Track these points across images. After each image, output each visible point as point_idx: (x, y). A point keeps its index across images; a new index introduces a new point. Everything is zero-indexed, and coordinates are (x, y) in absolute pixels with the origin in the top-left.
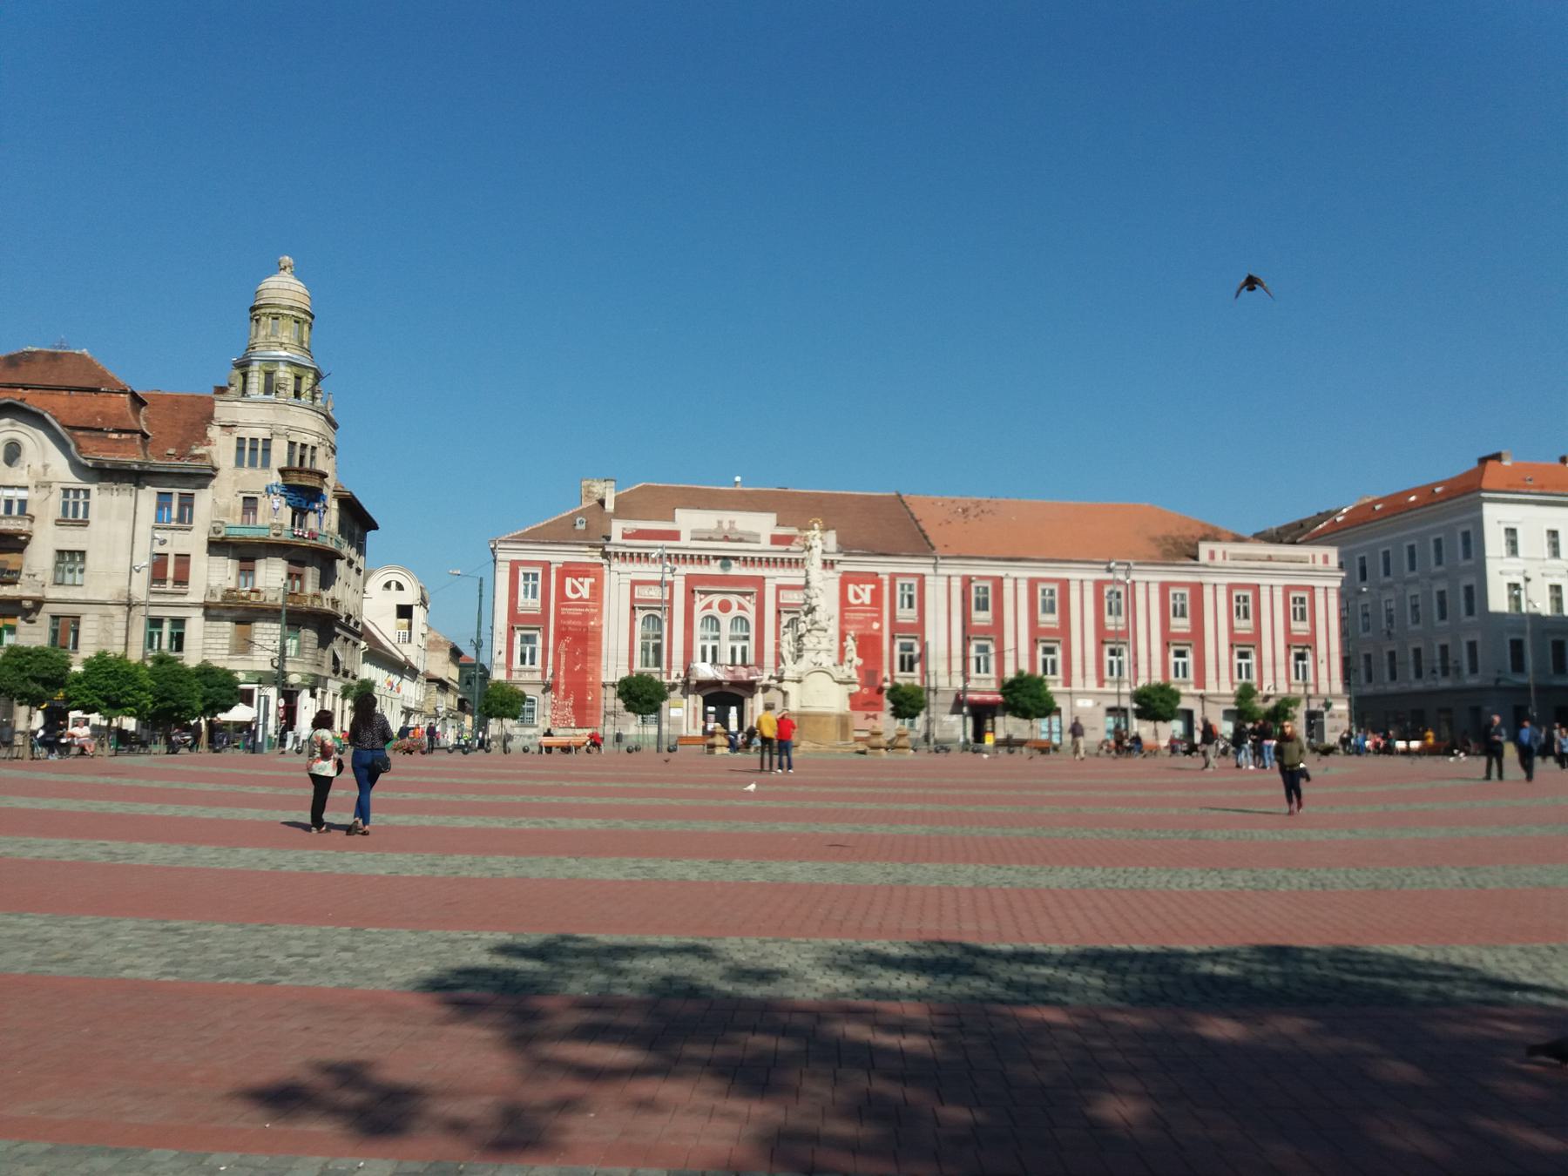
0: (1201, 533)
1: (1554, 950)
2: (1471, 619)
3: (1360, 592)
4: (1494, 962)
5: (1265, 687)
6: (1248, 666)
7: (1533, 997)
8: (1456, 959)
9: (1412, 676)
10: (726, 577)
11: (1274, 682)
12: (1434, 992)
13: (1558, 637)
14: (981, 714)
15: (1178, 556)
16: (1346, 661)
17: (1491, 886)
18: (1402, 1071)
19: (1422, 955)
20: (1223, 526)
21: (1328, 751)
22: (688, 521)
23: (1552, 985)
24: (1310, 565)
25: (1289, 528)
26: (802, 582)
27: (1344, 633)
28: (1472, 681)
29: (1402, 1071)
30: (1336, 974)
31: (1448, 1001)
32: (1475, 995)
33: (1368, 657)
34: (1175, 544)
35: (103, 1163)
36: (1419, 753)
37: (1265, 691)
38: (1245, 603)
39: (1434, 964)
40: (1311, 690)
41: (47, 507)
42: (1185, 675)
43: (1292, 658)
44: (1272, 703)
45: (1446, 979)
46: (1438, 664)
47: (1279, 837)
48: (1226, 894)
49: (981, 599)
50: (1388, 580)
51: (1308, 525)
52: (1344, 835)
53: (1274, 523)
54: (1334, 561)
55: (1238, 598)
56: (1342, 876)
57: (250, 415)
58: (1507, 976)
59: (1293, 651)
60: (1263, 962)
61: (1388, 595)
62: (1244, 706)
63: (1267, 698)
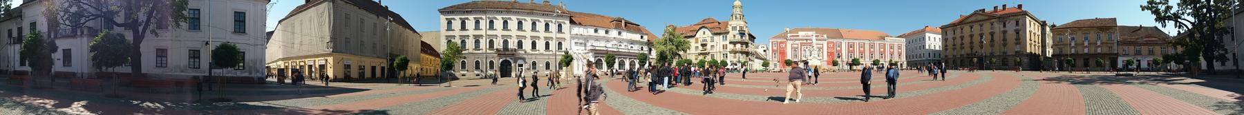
10: (807, 43)
11: (896, 59)
14: (851, 65)
22: (801, 33)
26: (525, 95)
35: (49, 103)
41: (709, 40)
49: (851, 46)
57: (733, 23)
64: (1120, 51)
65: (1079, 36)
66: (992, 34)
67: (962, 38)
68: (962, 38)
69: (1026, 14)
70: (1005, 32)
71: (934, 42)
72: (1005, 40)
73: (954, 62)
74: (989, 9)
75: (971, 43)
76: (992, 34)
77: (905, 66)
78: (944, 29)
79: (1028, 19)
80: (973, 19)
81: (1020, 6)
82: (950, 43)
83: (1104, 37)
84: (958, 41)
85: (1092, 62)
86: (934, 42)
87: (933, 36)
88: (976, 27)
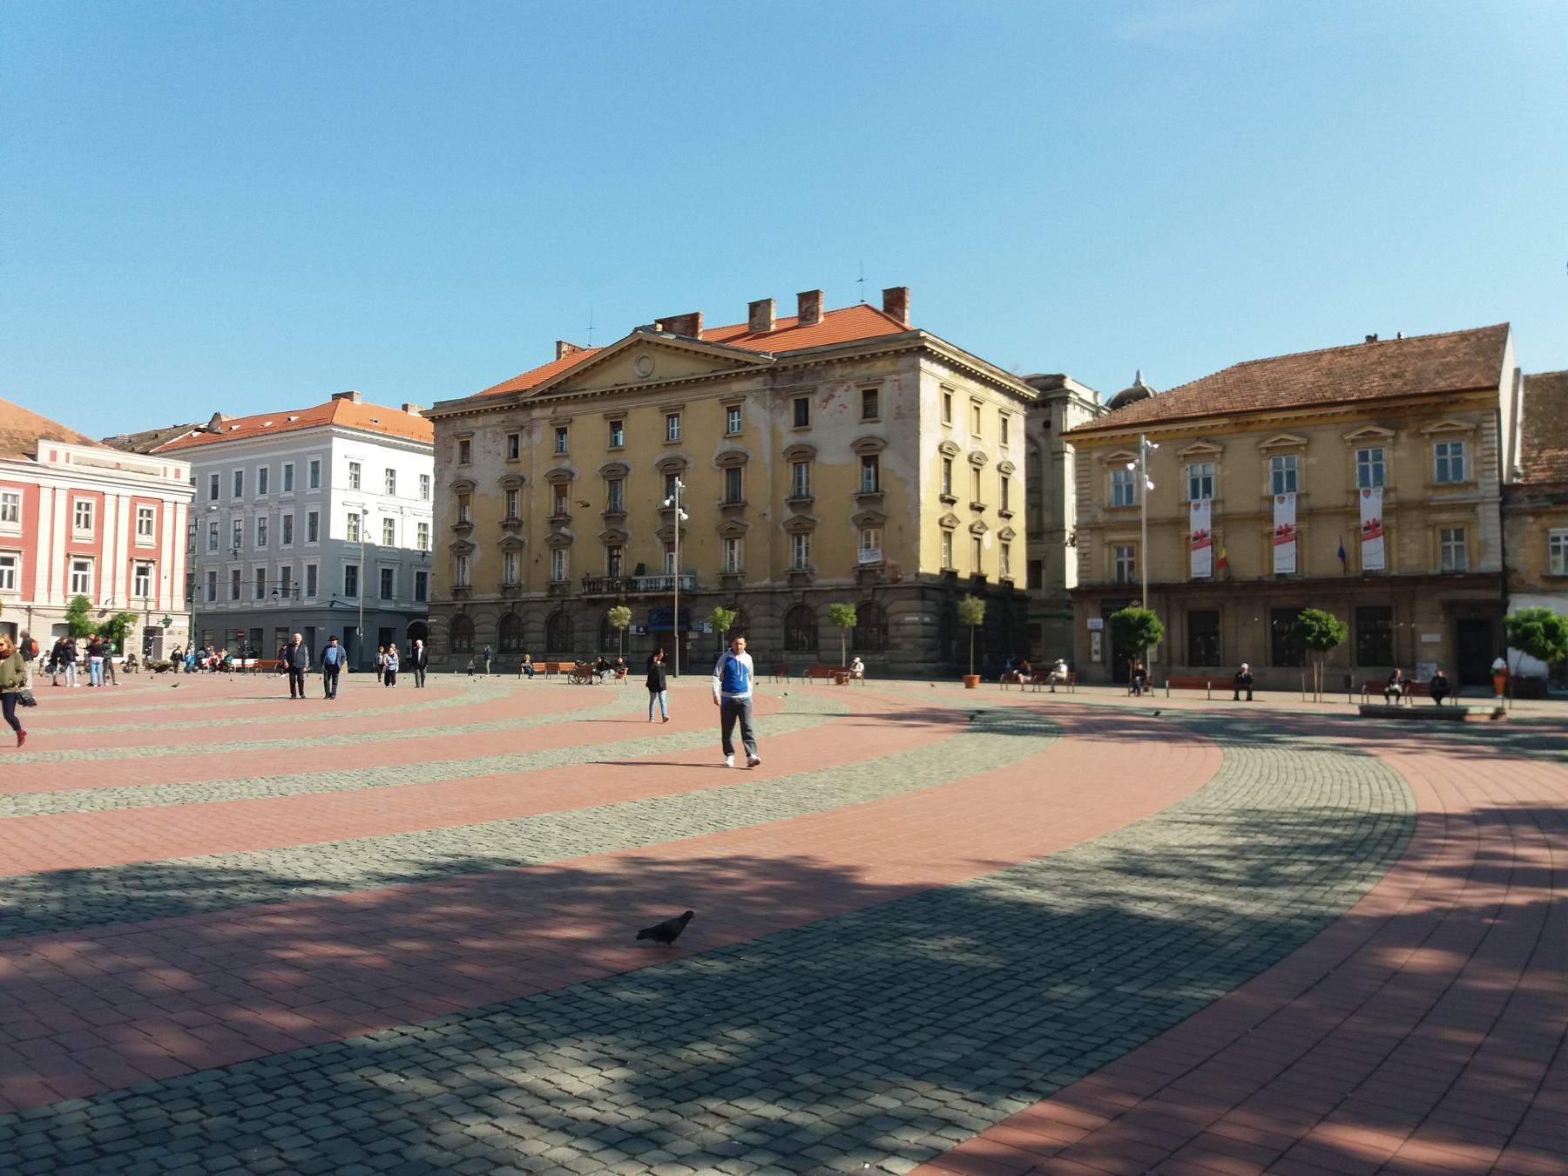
0: (43, 431)
1: (336, 847)
2: (313, 544)
3: (209, 511)
4: (280, 863)
5: (102, 601)
6: (84, 577)
7: (308, 891)
8: (246, 864)
9: (254, 595)
11: (112, 593)
12: (219, 898)
13: (387, 567)
15: (13, 452)
16: (190, 578)
17: (293, 793)
18: (175, 978)
19: (214, 864)
20: (72, 426)
21: (162, 668)
23: (328, 878)
24: (161, 478)
25: (142, 437)
27: (190, 550)
28: (309, 603)
29: (175, 978)
30: (124, 892)
31: (230, 904)
32: (258, 896)
33: (213, 575)
34: (11, 438)
36: (252, 670)
37: (102, 606)
38: (85, 512)
39: (225, 871)
40: (151, 606)
42: (10, 586)
43: (134, 572)
44: (108, 618)
45: (234, 883)
46: (280, 585)
47: (91, 757)
48: (17, 820)
50: (263, 497)
51: (162, 436)
52: (162, 751)
53: (126, 431)
54: (186, 477)
55: (79, 505)
56: (151, 793)
58: (290, 875)
59: (136, 565)
60: (45, 888)
61: (237, 515)
62: (76, 620)
63: (103, 612)
64: (1526, 559)
65: (1242, 471)
66: (733, 466)
67: (561, 482)
68: (561, 482)
69: (914, 348)
70: (802, 456)
71: (384, 498)
72: (801, 501)
73: (461, 628)
74: (721, 315)
75: (614, 515)
76: (733, 466)
77: (177, 637)
78: (453, 425)
79: (931, 378)
80: (627, 373)
81: (895, 300)
82: (487, 509)
83: (1407, 462)
84: (538, 502)
85: (1246, 634)
86: (384, 498)
87: (376, 459)
88: (644, 420)
